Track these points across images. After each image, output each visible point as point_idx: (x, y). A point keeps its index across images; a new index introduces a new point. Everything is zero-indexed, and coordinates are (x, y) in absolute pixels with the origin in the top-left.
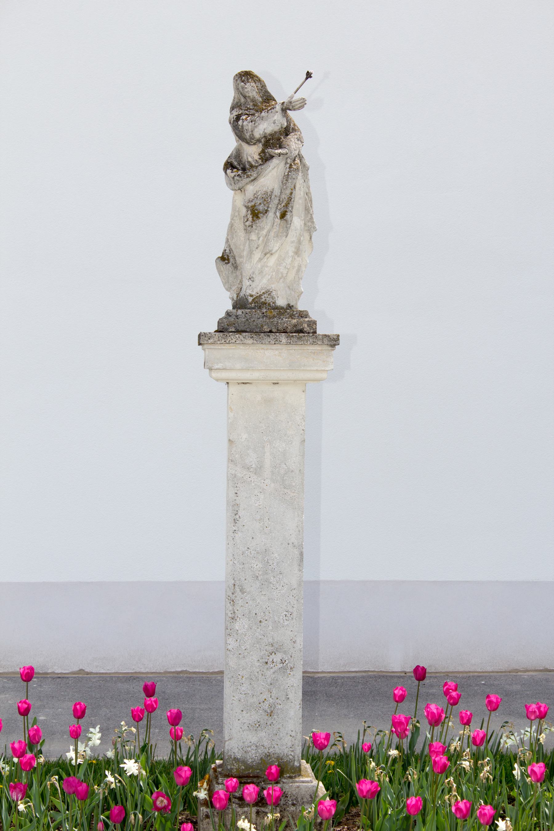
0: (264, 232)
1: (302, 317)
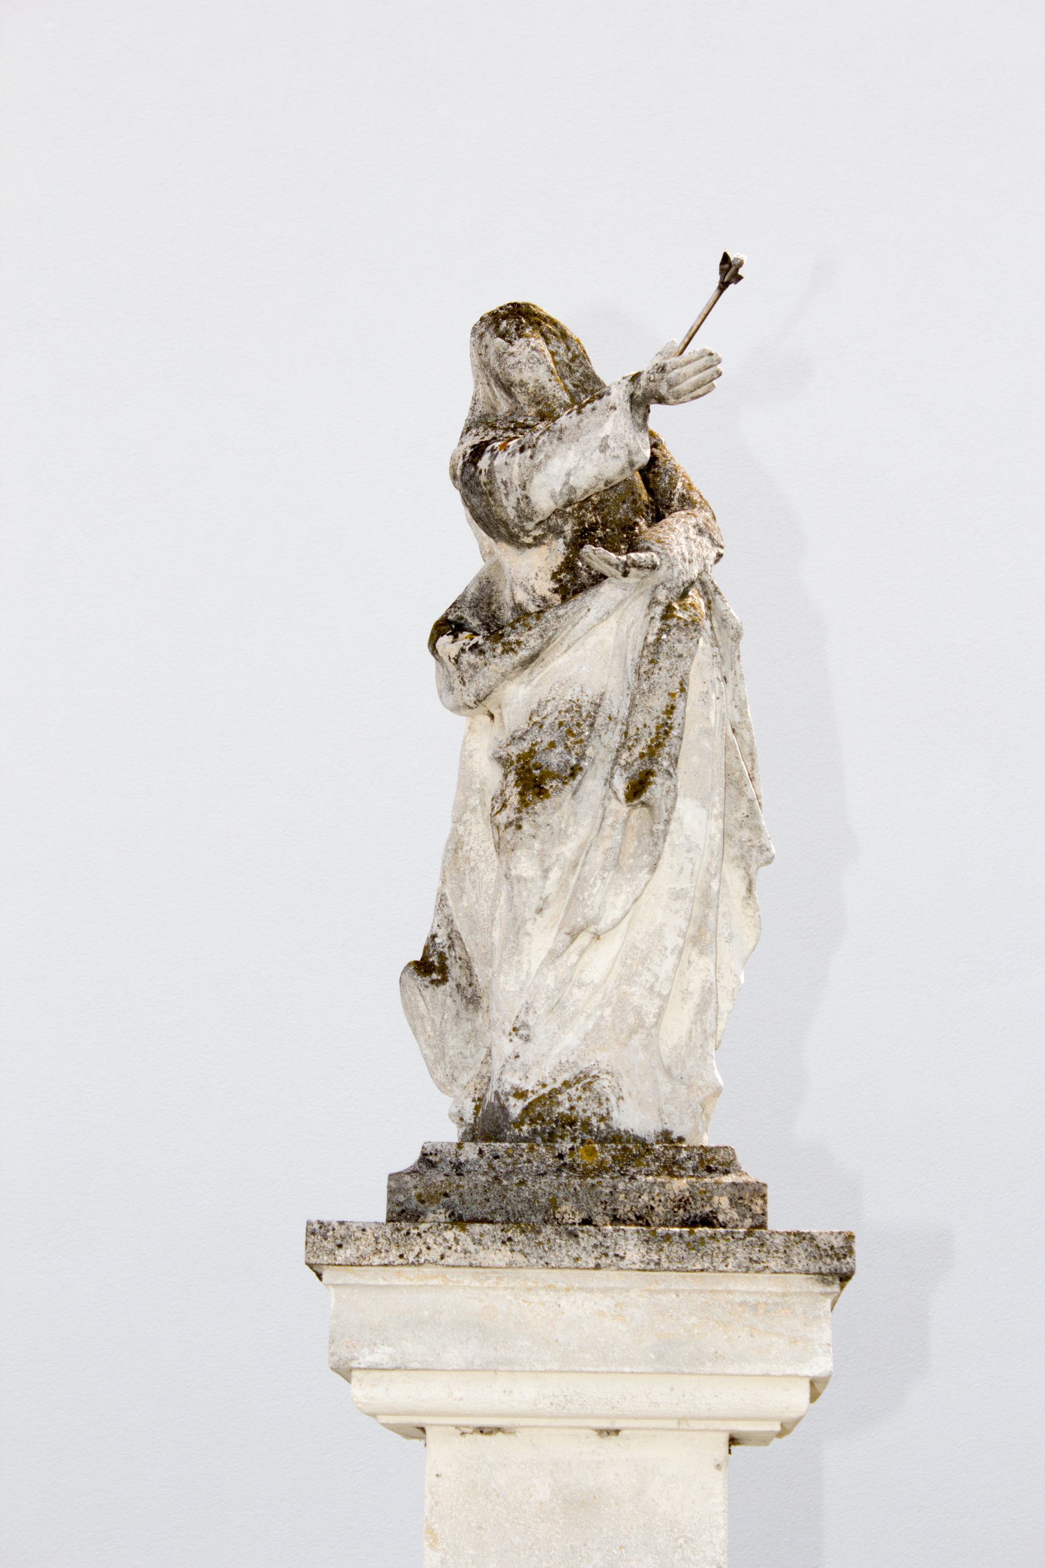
0: (568, 850)
1: (710, 1170)
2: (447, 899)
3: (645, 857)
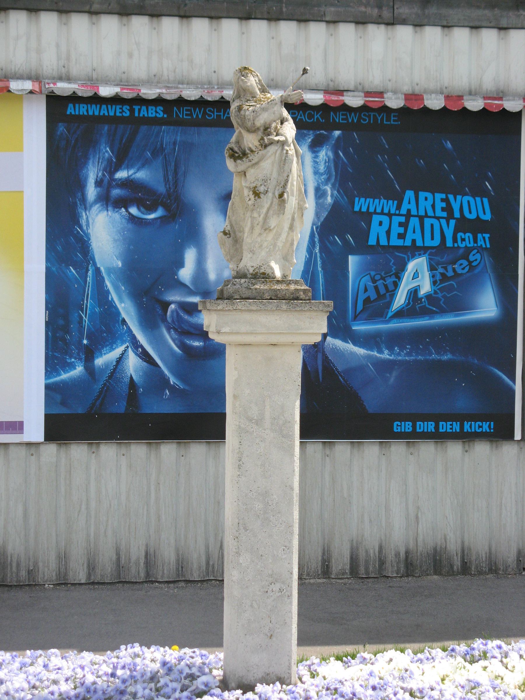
0: (264, 210)
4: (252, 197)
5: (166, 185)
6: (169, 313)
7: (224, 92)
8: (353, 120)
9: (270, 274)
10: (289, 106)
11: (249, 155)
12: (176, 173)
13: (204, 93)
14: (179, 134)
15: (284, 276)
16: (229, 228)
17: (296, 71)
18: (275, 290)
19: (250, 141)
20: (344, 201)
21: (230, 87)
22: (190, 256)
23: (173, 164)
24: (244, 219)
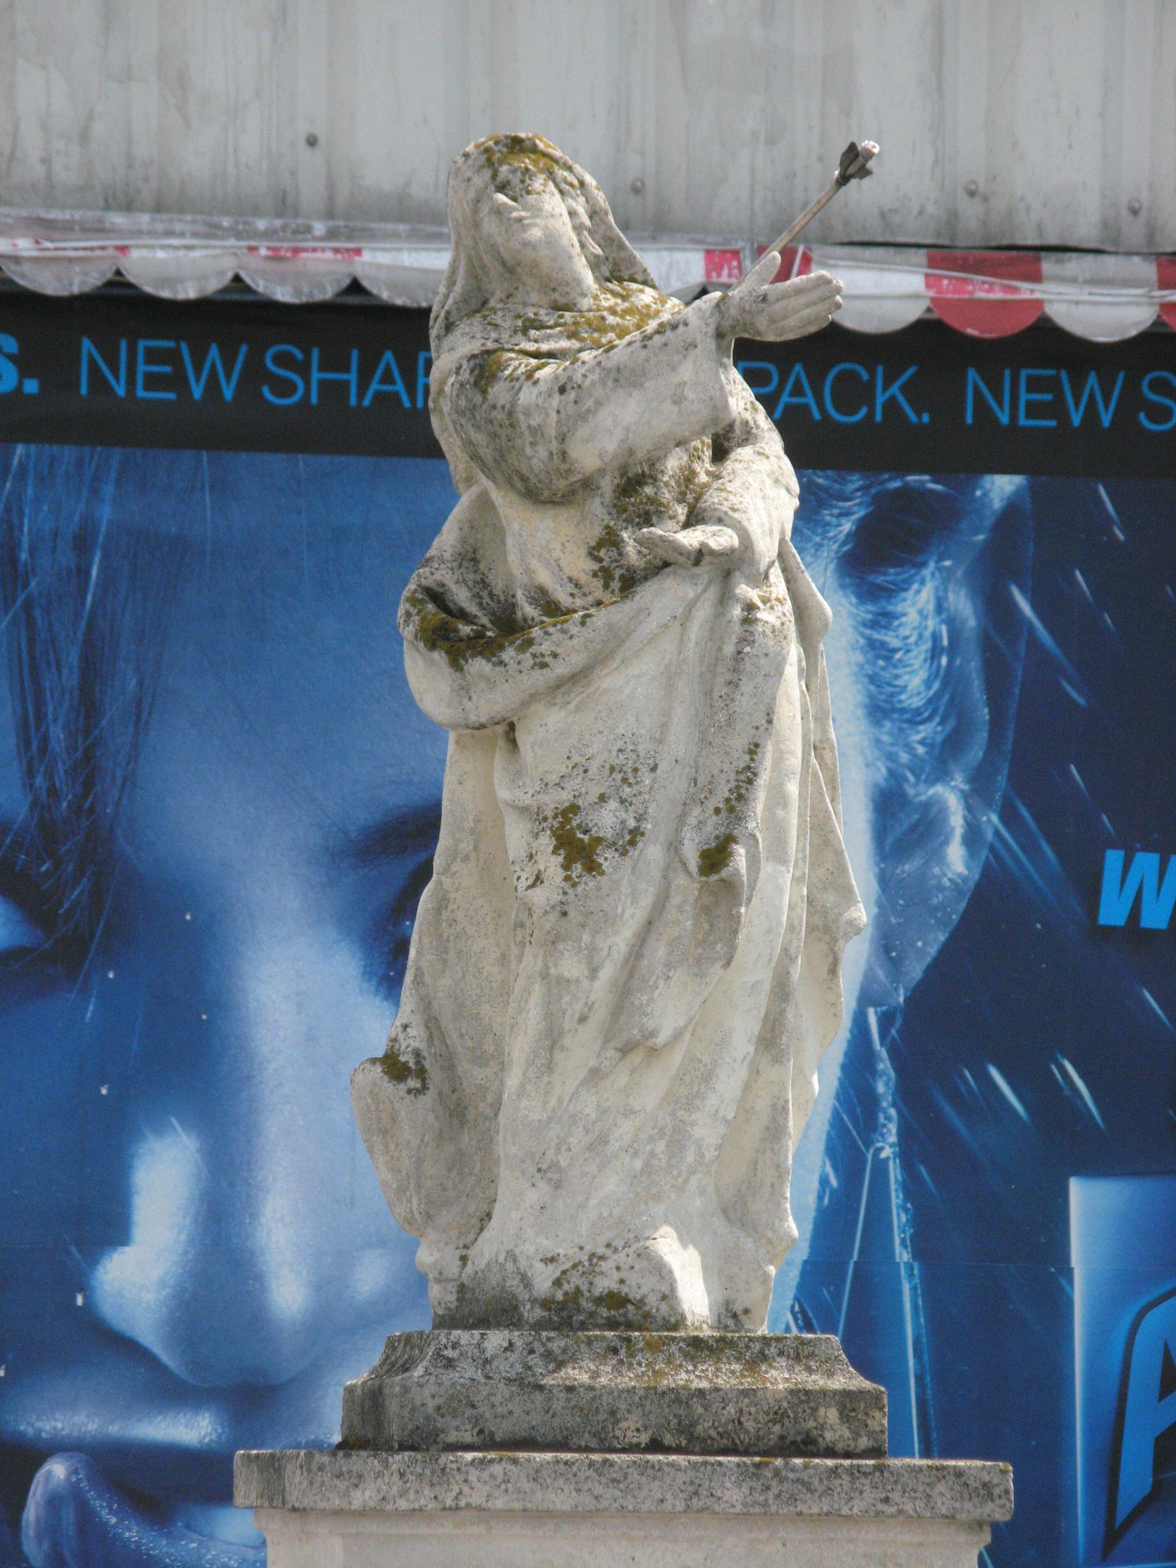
0: (621, 940)
2: (423, 974)
3: (719, 947)
4: (551, 864)
5: (30, 773)
6: (32, 1512)
7: (367, 256)
8: (1091, 413)
9: (652, 1300)
10: (755, 356)
11: (536, 632)
12: (88, 706)
13: (253, 262)
14: (108, 490)
15: (731, 1314)
16: (415, 1039)
17: (771, 141)
18: (680, 1397)
19: (544, 550)
20: (1040, 868)
21: (402, 227)
22: (163, 1178)
23: (73, 657)
24: (505, 990)
